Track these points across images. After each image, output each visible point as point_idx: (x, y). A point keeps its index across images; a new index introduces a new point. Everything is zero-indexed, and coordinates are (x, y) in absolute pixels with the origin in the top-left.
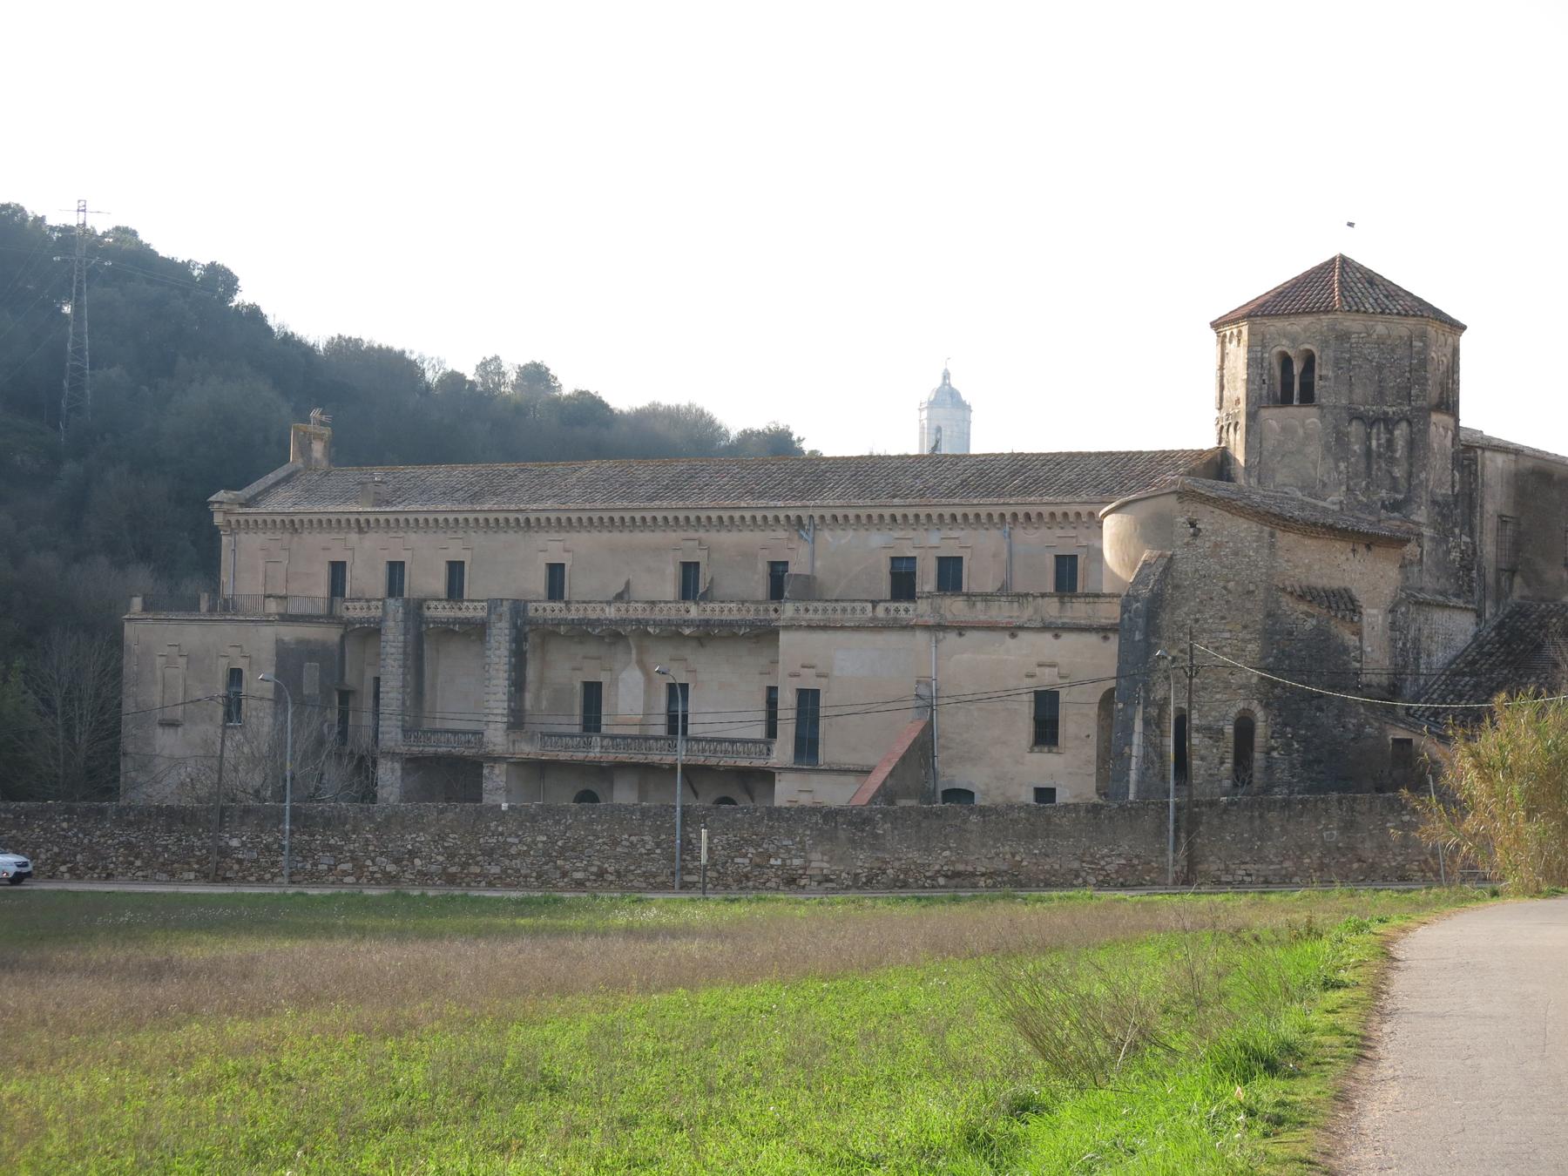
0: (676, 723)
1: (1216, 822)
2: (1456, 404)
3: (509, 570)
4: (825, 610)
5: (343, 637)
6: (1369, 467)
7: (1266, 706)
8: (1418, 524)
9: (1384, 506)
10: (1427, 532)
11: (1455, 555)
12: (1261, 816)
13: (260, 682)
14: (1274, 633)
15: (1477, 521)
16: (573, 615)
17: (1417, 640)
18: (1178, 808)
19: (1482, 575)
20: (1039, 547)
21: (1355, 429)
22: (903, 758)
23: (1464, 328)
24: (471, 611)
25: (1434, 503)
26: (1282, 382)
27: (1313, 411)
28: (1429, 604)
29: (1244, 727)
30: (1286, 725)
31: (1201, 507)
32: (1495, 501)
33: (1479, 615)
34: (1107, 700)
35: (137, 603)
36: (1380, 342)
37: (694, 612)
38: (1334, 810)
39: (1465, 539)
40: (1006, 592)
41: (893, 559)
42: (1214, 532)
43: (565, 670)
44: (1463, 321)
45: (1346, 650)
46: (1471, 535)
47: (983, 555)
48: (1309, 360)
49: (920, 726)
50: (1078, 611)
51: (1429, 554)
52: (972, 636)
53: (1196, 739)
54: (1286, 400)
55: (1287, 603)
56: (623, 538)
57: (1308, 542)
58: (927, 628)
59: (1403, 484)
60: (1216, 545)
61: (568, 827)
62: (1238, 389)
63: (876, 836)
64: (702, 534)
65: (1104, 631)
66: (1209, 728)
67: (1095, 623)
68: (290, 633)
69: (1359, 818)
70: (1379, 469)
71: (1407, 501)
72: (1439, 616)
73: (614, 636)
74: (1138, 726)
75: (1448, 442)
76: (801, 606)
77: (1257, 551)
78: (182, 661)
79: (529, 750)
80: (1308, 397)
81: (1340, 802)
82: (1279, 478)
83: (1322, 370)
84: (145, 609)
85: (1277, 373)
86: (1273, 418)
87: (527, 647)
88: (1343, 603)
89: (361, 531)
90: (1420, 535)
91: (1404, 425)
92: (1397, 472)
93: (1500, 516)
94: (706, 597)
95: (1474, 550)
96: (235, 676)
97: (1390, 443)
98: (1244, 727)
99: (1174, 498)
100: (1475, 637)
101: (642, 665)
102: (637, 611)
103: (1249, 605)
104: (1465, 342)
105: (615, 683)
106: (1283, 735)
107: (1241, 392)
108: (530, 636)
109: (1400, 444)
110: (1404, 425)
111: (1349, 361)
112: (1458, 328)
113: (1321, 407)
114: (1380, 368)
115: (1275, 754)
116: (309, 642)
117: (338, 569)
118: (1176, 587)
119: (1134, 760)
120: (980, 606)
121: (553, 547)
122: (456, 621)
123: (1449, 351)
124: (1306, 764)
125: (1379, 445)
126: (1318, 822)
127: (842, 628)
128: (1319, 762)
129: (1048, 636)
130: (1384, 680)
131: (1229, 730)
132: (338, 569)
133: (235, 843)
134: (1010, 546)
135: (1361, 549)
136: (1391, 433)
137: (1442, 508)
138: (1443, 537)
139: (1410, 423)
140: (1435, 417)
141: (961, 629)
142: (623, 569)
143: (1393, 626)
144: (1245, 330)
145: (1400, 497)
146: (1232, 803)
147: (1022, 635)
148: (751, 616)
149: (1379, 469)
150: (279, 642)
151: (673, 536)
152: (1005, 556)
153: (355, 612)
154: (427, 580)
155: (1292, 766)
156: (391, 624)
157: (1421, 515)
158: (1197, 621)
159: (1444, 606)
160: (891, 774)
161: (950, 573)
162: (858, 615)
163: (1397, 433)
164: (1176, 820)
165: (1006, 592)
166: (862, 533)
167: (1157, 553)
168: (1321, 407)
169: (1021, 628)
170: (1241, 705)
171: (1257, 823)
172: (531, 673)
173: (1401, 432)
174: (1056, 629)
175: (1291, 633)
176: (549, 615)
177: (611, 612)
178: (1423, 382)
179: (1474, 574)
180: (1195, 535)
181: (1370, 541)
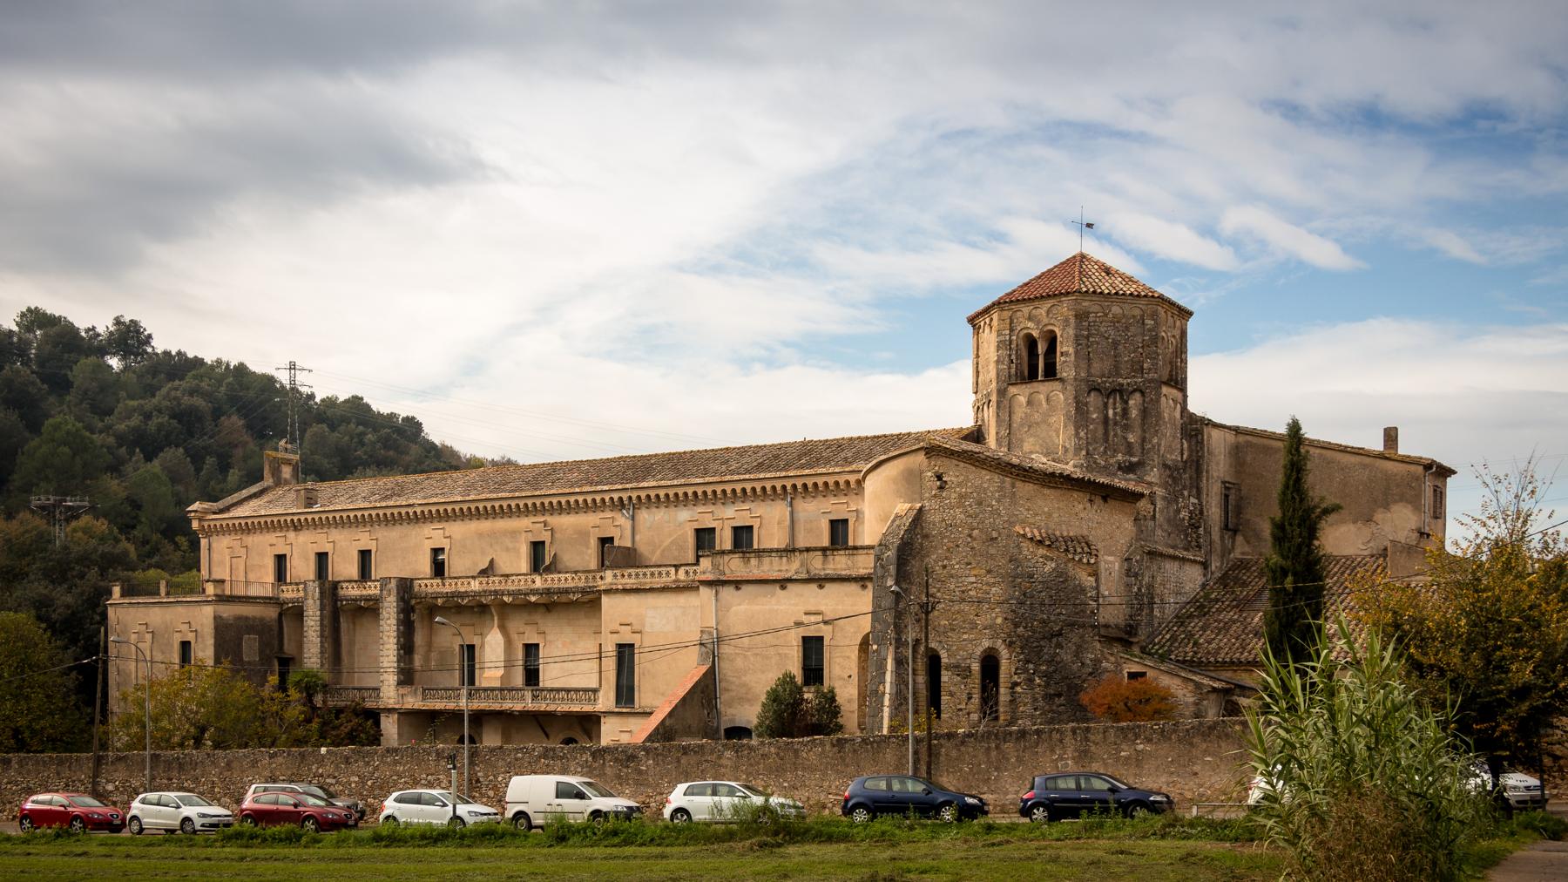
0: (532, 676)
1: (954, 753)
2: (1184, 380)
3: (405, 555)
4: (637, 575)
5: (280, 615)
6: (1106, 433)
7: (1010, 645)
8: (1150, 484)
9: (1120, 468)
10: (1160, 492)
11: (1184, 514)
12: (997, 747)
13: (205, 651)
14: (1018, 576)
15: (1204, 484)
16: (447, 589)
17: (1150, 586)
18: (917, 741)
19: (1208, 532)
20: (816, 515)
21: (1093, 399)
22: (684, 699)
23: (1191, 314)
24: (372, 589)
25: (1165, 466)
26: (1032, 362)
27: (1057, 385)
28: (1161, 555)
29: (990, 664)
30: (1028, 662)
31: (947, 461)
32: (1219, 467)
33: (1205, 565)
34: (864, 644)
35: (117, 590)
36: (1115, 321)
37: (539, 582)
38: (1068, 740)
39: (1193, 500)
40: (789, 551)
41: (697, 531)
42: (959, 485)
43: (449, 637)
44: (1190, 308)
45: (1083, 591)
46: (1198, 497)
47: (770, 521)
48: (1052, 341)
49: (704, 669)
50: (840, 563)
51: (1161, 511)
52: (747, 590)
53: (945, 677)
54: (1032, 376)
55: (1027, 549)
56: (486, 525)
57: (1046, 491)
58: (709, 583)
59: (1137, 448)
60: (961, 496)
61: (376, 769)
62: (990, 373)
63: (640, 772)
64: (548, 518)
65: (862, 580)
66: (957, 666)
67: (854, 573)
68: (228, 611)
69: (1093, 748)
70: (1115, 435)
71: (1141, 464)
72: (1171, 567)
73: (478, 609)
74: (890, 664)
75: (1178, 414)
76: (618, 572)
77: (998, 501)
78: (149, 636)
79: (414, 702)
80: (1051, 372)
81: (1074, 731)
82: (1027, 447)
83: (1065, 347)
84: (123, 595)
85: (1025, 354)
86: (1020, 394)
87: (414, 617)
88: (1080, 547)
89: (296, 529)
90: (1152, 494)
91: (1138, 395)
92: (1131, 438)
93: (1224, 482)
94: (548, 570)
95: (1201, 512)
96: (185, 646)
97: (1125, 412)
98: (990, 664)
99: (921, 457)
100: (1204, 586)
101: (503, 628)
102: (494, 583)
103: (992, 551)
104: (1192, 326)
105: (483, 645)
106: (1026, 671)
107: (993, 374)
108: (415, 609)
109: (1134, 413)
110: (1138, 395)
111: (1087, 337)
112: (1185, 314)
113: (1061, 380)
114: (1115, 344)
115: (1018, 689)
116: (247, 618)
117: (281, 560)
118: (926, 536)
119: (887, 697)
120: (753, 561)
121: (433, 535)
122: (362, 598)
123: (1177, 333)
124: (1049, 698)
126: (1053, 751)
127: (651, 590)
128: (1059, 695)
129: (814, 587)
130: (1121, 621)
131: (976, 667)
132: (281, 560)
133: (110, 787)
134: (792, 513)
135: (1098, 501)
137: (1173, 473)
138: (1173, 498)
139: (1143, 394)
140: (1165, 390)
141: (737, 584)
142: (490, 552)
143: (1128, 573)
144: (995, 317)
145: (1134, 460)
146: (970, 735)
147: (790, 586)
148: (581, 584)
149: (1115, 435)
150: (217, 618)
151: (526, 522)
152: (788, 522)
153: (288, 593)
154: (345, 567)
155: (1035, 700)
156: (310, 601)
157: (1154, 475)
158: (944, 567)
159: (1175, 558)
160: (670, 714)
161: (742, 535)
162: (665, 579)
163: (1131, 402)
164: (916, 753)
165: (789, 551)
166: (672, 510)
167: (908, 506)
168: (1061, 380)
169: (790, 580)
170: (986, 644)
171: (994, 753)
172: (419, 639)
173: (1135, 402)
174: (821, 581)
176: (430, 590)
177: (475, 586)
178: (1154, 357)
179: (1201, 531)
180: (941, 488)
181: (1107, 494)
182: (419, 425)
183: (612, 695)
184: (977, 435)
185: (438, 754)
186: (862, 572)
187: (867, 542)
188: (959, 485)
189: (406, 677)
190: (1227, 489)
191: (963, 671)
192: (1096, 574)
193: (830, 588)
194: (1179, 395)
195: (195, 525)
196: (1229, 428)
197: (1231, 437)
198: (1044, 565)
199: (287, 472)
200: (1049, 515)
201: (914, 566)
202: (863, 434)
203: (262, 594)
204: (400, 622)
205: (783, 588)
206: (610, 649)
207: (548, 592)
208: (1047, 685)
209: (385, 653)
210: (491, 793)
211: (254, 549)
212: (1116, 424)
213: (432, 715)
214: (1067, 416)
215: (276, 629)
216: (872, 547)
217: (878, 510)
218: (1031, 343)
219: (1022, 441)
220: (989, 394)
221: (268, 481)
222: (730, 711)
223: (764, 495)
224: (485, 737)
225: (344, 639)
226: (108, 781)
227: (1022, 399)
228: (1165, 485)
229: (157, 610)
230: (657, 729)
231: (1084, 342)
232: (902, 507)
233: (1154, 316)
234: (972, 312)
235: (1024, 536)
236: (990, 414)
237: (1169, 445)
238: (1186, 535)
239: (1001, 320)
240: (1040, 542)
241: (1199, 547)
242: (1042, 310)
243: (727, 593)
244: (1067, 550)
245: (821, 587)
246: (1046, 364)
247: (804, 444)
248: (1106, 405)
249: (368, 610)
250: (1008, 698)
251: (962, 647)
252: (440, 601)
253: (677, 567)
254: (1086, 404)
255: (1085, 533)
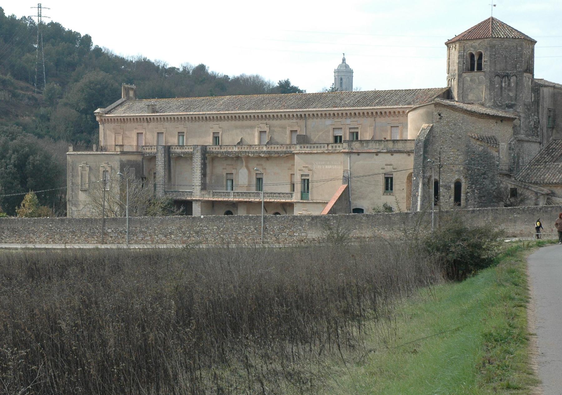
11: (532, 123)
14: (469, 152)
23: (536, 42)
25: (525, 104)
26: (471, 63)
29: (458, 185)
31: (442, 109)
32: (546, 103)
39: (535, 117)
42: (447, 117)
43: (221, 169)
44: (536, 39)
45: (494, 157)
48: (480, 55)
49: (346, 186)
51: (523, 123)
53: (441, 190)
54: (472, 69)
55: (473, 142)
57: (480, 120)
60: (448, 122)
64: (267, 121)
65: (409, 153)
68: (125, 158)
75: (530, 83)
76: (302, 146)
77: (462, 124)
78: (87, 169)
80: (480, 68)
85: (469, 60)
86: (468, 76)
88: (492, 141)
98: (458, 185)
103: (459, 142)
104: (536, 46)
106: (471, 188)
107: (456, 67)
108: (208, 157)
109: (513, 85)
110: (515, 77)
111: (495, 55)
112: (534, 42)
115: (469, 194)
121: (215, 127)
123: (530, 50)
124: (480, 197)
125: (505, 85)
126: (484, 217)
129: (389, 155)
131: (453, 186)
133: (109, 231)
135: (499, 122)
136: (510, 80)
137: (528, 107)
138: (527, 117)
140: (525, 74)
144: (458, 45)
150: (121, 161)
155: (475, 198)
156: (159, 154)
157: (520, 109)
158: (441, 148)
160: (335, 204)
163: (512, 80)
165: (373, 140)
166: (323, 120)
167: (427, 125)
170: (457, 177)
172: (208, 171)
173: (513, 79)
174: (392, 152)
175: (474, 152)
177: (236, 149)
180: (440, 118)
182: (90, 37)
183: (299, 195)
184: (447, 94)
185: (250, 218)
186: (409, 149)
187: (409, 138)
188: (447, 117)
189: (204, 187)
190: (550, 111)
191: (447, 188)
192: (498, 151)
193: (396, 155)
194: (531, 75)
195: (98, 119)
196: (551, 87)
197: (551, 90)
198: (479, 147)
199: (131, 93)
200: (481, 128)
201: (429, 148)
202: (401, 89)
203: (131, 150)
204: (202, 164)
205: (377, 155)
206: (297, 179)
207: (269, 152)
208: (480, 193)
209: (195, 176)
210: (272, 233)
211: (125, 130)
212: (505, 89)
213: (213, 203)
214: (486, 86)
215: (141, 164)
216: (414, 140)
217: (414, 126)
218: (472, 56)
219: (468, 95)
220: (454, 75)
221: (123, 99)
222: (355, 202)
223: (364, 115)
224: (239, 212)
225: (172, 171)
226: (108, 228)
227: (469, 79)
228: (525, 113)
229: (92, 157)
230: (331, 209)
231: (493, 57)
232: (425, 125)
233: (521, 46)
234: (451, 37)
235: (472, 137)
236: (455, 83)
237: (527, 96)
238: (533, 131)
239: (460, 47)
240: (478, 139)
241: (538, 136)
242: (476, 43)
243: (354, 157)
244: (488, 143)
245: (392, 155)
246: (478, 64)
247: (375, 92)
248: (502, 82)
249: (189, 157)
250: (465, 197)
251: (448, 179)
252: (219, 155)
253: (328, 144)
254: (494, 81)
255: (494, 134)
